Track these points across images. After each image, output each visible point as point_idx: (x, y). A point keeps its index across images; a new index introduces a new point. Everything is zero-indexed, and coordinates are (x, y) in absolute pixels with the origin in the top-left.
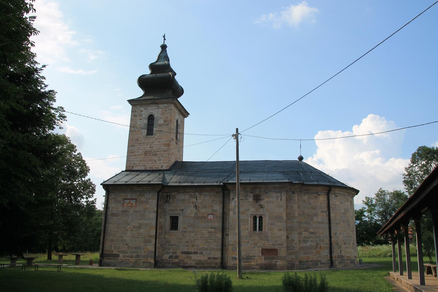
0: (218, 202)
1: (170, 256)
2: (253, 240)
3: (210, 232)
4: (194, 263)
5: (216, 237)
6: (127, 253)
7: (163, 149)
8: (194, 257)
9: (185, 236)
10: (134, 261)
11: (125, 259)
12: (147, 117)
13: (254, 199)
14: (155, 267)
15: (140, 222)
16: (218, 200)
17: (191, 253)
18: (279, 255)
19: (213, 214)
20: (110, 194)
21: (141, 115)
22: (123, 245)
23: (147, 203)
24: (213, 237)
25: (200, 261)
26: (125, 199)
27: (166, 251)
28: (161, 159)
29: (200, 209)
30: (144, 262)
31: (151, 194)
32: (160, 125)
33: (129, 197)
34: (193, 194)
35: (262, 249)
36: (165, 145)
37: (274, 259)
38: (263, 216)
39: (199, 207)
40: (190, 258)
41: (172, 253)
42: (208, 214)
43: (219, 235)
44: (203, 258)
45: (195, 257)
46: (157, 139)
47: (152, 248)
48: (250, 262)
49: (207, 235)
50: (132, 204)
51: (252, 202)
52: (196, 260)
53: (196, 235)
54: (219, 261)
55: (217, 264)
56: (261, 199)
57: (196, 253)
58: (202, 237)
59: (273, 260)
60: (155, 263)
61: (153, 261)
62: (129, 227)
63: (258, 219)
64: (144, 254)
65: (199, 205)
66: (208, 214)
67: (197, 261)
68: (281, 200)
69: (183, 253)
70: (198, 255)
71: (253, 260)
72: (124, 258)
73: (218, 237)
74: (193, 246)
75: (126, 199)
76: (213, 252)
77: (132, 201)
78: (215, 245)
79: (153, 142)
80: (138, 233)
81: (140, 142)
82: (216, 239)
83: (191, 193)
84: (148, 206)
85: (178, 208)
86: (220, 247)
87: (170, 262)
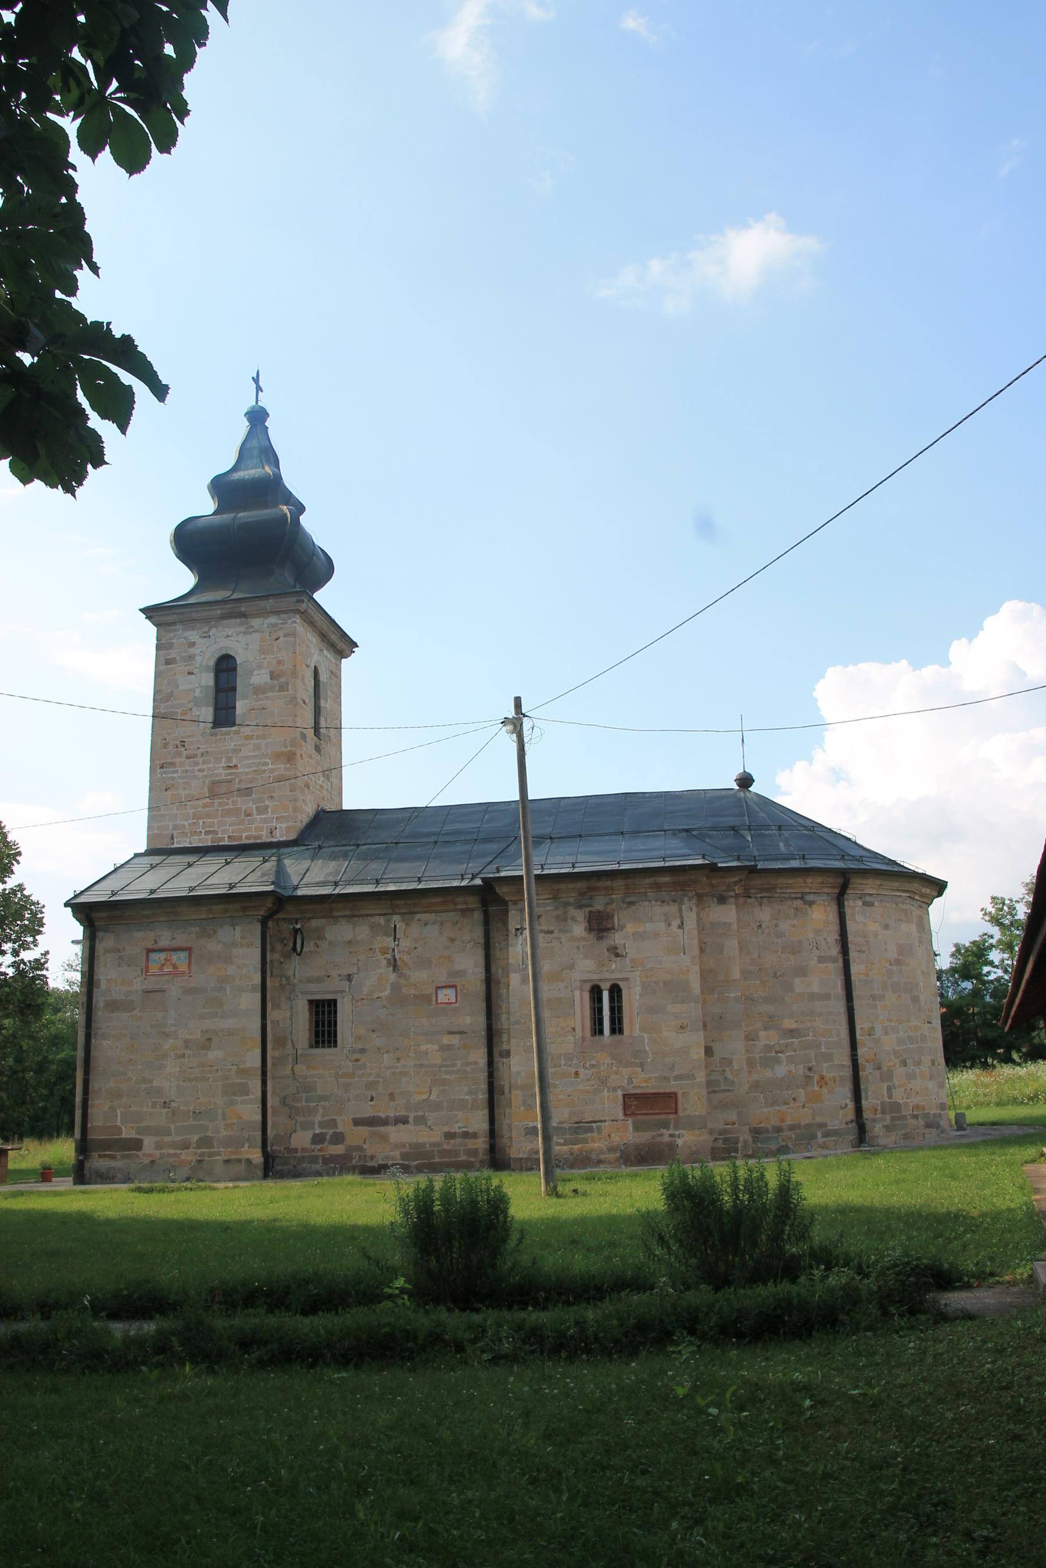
1: (315, 1136)
3: (444, 1048)
4: (397, 1154)
5: (467, 1064)
7: (272, 771)
8: (397, 1134)
10: (194, 1158)
12: (212, 663)
13: (590, 929)
14: (266, 1176)
17: (385, 1122)
18: (681, 1114)
20: (100, 934)
21: (191, 658)
22: (154, 1105)
23: (228, 960)
24: (459, 1063)
25: (418, 1146)
26: (149, 951)
27: (300, 1119)
28: (267, 807)
29: (408, 973)
30: (227, 1161)
31: (238, 929)
32: (259, 690)
33: (164, 943)
34: (382, 920)
35: (624, 1096)
36: (277, 757)
38: (622, 984)
39: (406, 964)
40: (384, 1138)
41: (322, 1125)
42: (438, 988)
43: (479, 1056)
46: (248, 738)
50: (175, 967)
51: (583, 939)
52: (404, 1146)
53: (399, 1059)
54: (481, 1144)
55: (474, 1152)
56: (613, 928)
57: (404, 1121)
58: (421, 1066)
59: (664, 1131)
61: (260, 1155)
63: (606, 995)
64: (225, 1133)
65: (406, 958)
66: (438, 988)
67: (407, 1149)
68: (681, 926)
69: (357, 1122)
70: (410, 1127)
71: (595, 1134)
72: (157, 1153)
75: (154, 951)
76: (460, 1114)
77: (175, 957)
78: (466, 1089)
79: (236, 751)
81: (190, 753)
82: (468, 1069)
84: (231, 970)
85: (334, 973)
86: (482, 1096)
87: (317, 1157)
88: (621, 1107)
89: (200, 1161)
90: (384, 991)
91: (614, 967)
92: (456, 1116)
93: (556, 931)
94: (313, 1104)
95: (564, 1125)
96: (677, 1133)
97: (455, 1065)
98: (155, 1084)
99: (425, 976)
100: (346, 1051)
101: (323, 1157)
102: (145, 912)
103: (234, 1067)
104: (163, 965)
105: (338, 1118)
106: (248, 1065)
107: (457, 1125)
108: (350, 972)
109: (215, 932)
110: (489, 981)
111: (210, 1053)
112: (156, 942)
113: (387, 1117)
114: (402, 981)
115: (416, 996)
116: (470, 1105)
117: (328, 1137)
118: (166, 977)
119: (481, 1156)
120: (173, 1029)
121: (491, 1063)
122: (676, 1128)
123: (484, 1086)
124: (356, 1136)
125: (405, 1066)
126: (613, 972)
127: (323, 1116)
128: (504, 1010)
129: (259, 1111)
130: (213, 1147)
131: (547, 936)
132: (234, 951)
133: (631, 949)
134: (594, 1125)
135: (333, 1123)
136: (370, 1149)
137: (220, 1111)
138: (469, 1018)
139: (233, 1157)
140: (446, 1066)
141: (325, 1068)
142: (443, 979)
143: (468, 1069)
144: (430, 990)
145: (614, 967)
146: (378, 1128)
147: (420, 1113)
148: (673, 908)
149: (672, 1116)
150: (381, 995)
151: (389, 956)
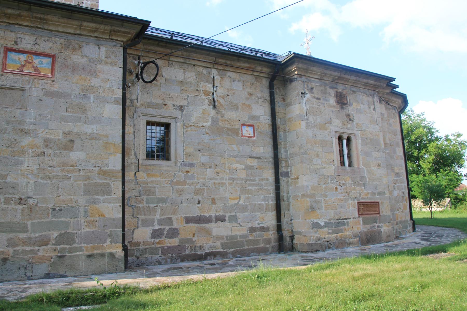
0: (261, 100)
1: (155, 231)
2: (344, 184)
3: (248, 168)
4: (218, 244)
5: (262, 180)
6: (24, 229)
8: (218, 229)
9: (193, 177)
10: (54, 254)
11: (16, 253)
13: (338, 102)
14: (125, 271)
15: (71, 127)
16: (259, 95)
17: (208, 220)
18: (381, 214)
19: (253, 126)
22: (7, 201)
23: (93, 73)
24: (257, 179)
25: (232, 237)
26: (8, 50)
27: (141, 217)
29: (223, 112)
30: (90, 256)
31: (103, 49)
34: (205, 71)
35: (358, 203)
37: (376, 222)
38: (353, 137)
39: (222, 105)
40: (208, 232)
41: (160, 222)
42: (243, 125)
43: (269, 175)
44: (238, 230)
45: (219, 230)
47: (112, 210)
48: (341, 231)
49: (243, 175)
50: (36, 69)
51: (334, 107)
52: (222, 238)
53: (218, 173)
54: (272, 235)
55: (268, 241)
56: (347, 104)
57: (222, 219)
58: (233, 179)
59: (375, 224)
60: (126, 256)
61: (120, 249)
62: (26, 141)
63: (345, 142)
64: (87, 229)
65: (221, 100)
66: (243, 125)
67: (225, 240)
68: (374, 109)
69: (188, 220)
70: (227, 223)
71: (346, 227)
72: (11, 250)
73: (267, 179)
74: (213, 201)
76: (259, 214)
77: (37, 61)
78: (262, 197)
80: (65, 165)
82: (263, 183)
83: (201, 69)
84: (95, 82)
85: (170, 103)
86: (272, 202)
87: (157, 248)
88: (357, 210)
89: (60, 257)
90: (206, 122)
91: (349, 126)
92: (256, 215)
93: (322, 99)
94: (152, 206)
95: (332, 221)
96: (380, 225)
97: (254, 180)
98: (9, 180)
99: (235, 116)
100: (179, 165)
101: (162, 248)
102: (9, 11)
103: (97, 169)
104: (23, 66)
105: (174, 217)
106: (111, 167)
107: (257, 222)
108: (182, 104)
109: (80, 47)
110: (274, 125)
111: (71, 153)
112: (16, 43)
113: (210, 216)
114: (219, 117)
115: (228, 129)
116: (265, 208)
117: (165, 232)
118: (27, 78)
119: (273, 244)
120: (32, 127)
121: (277, 180)
122: (380, 223)
123: (272, 195)
124: (187, 231)
125: (222, 179)
126: (348, 130)
127: (161, 215)
128: (283, 146)
129: (120, 209)
130: (74, 243)
131: (317, 101)
132: (99, 66)
133: (356, 117)
134: (346, 221)
135: (169, 221)
136: (199, 240)
137: (82, 209)
138: (262, 148)
139: (95, 252)
140: (249, 180)
141: (158, 178)
142: (245, 120)
143: (263, 183)
144: (237, 126)
145: (349, 126)
146: (204, 225)
147: (233, 214)
148: (371, 99)
149: (378, 215)
150: (205, 124)
151: (210, 97)
